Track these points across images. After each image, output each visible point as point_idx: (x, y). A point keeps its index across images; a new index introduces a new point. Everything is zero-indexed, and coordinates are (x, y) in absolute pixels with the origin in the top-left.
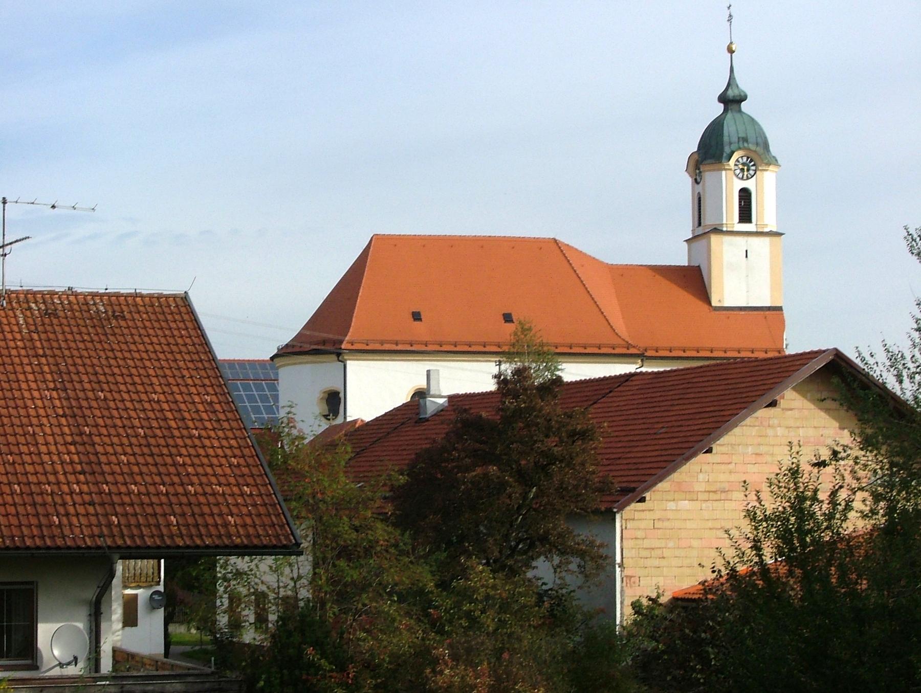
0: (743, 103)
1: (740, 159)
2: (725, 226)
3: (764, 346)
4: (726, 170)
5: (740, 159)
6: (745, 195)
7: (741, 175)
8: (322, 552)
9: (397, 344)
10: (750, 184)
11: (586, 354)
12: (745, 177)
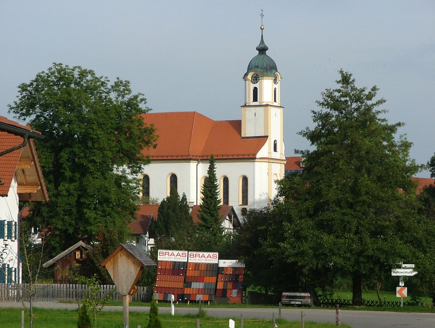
0: (267, 51)
1: (254, 75)
2: (247, 103)
3: (243, 153)
4: (247, 80)
5: (254, 75)
6: (255, 90)
7: (254, 82)
8: (423, 289)
9: (172, 157)
10: (257, 85)
11: (173, 159)
12: (255, 82)
